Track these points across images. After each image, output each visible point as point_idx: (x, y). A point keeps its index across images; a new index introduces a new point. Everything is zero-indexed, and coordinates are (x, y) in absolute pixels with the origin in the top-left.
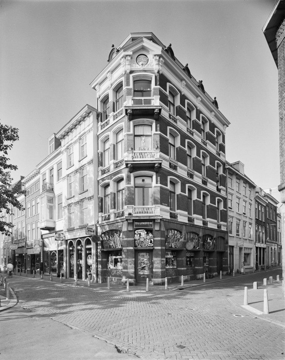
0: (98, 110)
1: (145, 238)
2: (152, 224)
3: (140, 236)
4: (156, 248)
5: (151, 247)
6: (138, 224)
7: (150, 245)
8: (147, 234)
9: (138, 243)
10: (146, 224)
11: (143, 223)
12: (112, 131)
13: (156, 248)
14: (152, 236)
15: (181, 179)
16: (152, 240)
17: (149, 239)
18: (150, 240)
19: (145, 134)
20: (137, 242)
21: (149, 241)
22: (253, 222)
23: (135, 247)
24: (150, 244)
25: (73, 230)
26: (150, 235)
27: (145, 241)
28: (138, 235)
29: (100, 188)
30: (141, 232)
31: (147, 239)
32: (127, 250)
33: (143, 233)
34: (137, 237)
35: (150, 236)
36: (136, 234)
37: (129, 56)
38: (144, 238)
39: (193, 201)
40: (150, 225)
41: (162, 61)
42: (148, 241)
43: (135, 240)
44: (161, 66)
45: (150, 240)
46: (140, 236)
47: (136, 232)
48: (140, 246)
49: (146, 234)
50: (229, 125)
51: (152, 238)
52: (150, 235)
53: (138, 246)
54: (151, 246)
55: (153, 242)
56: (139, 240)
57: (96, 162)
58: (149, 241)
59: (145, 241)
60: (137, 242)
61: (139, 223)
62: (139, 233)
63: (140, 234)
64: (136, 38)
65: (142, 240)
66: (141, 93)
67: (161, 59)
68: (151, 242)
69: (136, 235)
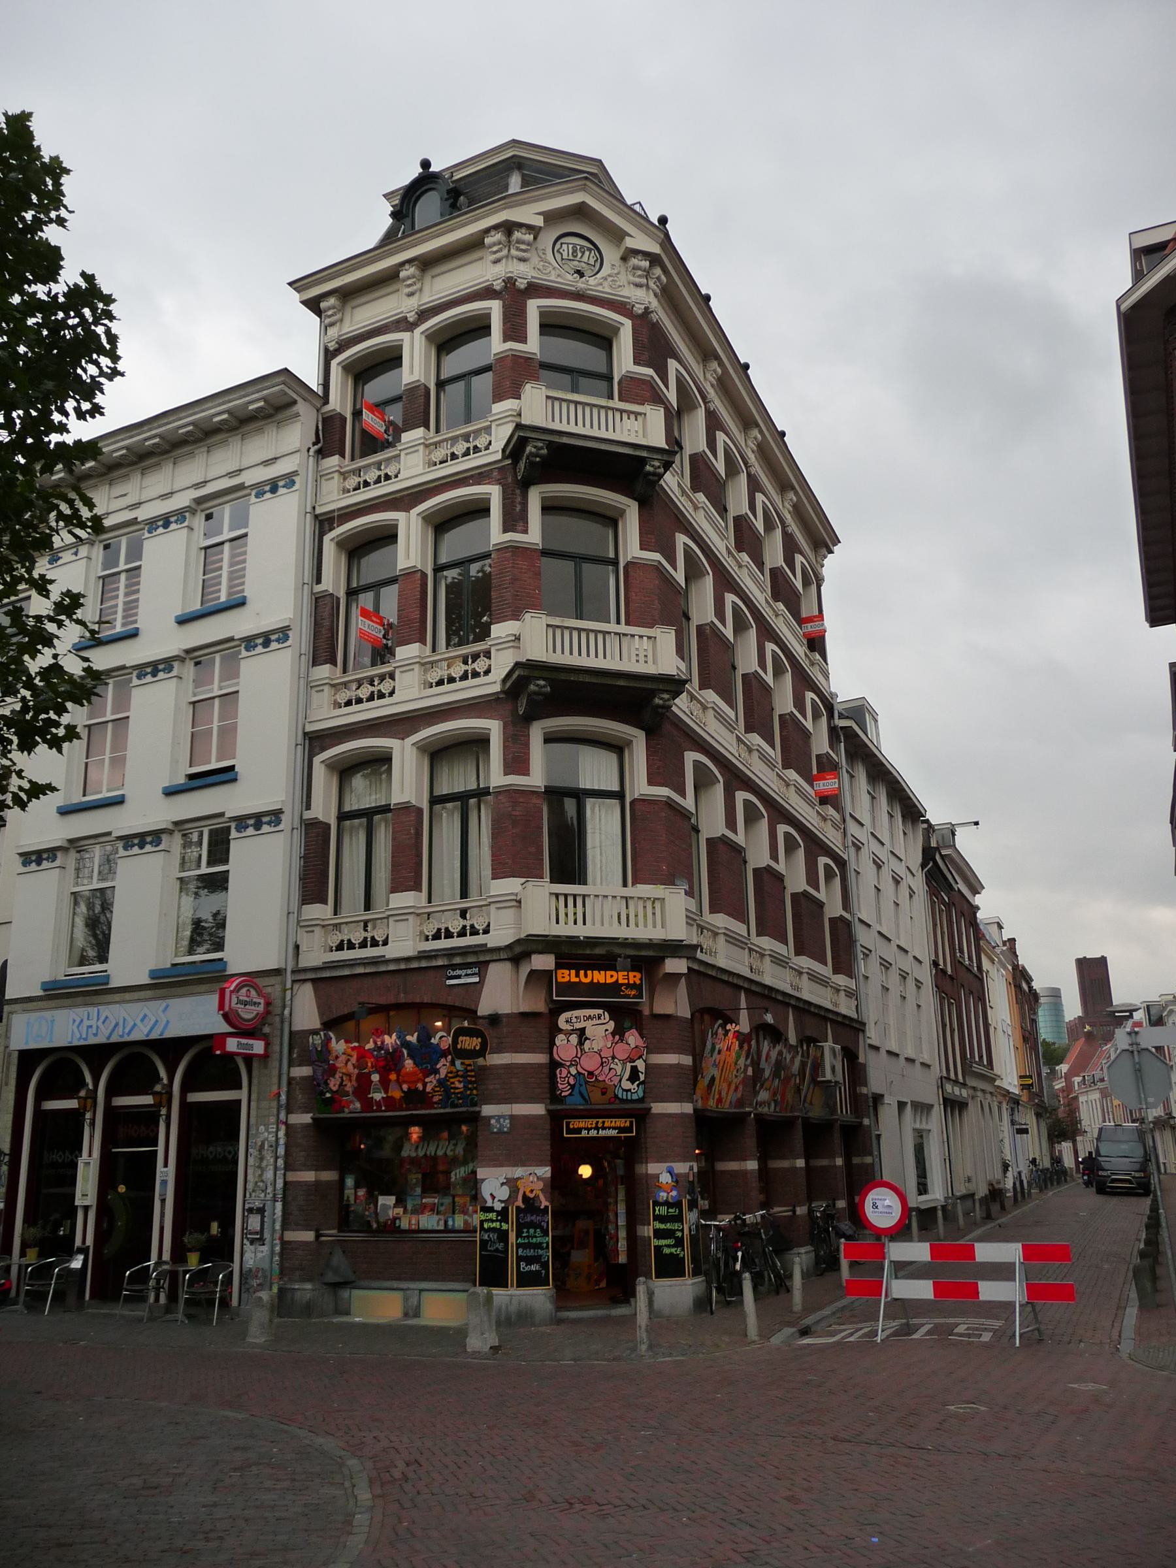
0: (326, 399)
1: (607, 1054)
2: (638, 982)
3: (581, 1043)
4: (658, 1108)
5: (632, 1101)
6: (574, 979)
7: (627, 1091)
8: (619, 1032)
9: (572, 1082)
10: (609, 981)
11: (596, 972)
12: (415, 511)
13: (658, 1108)
14: (641, 1043)
15: (730, 770)
16: (640, 1065)
17: (624, 1062)
18: (629, 1065)
19: (245, 464)
20: (565, 1072)
21: (624, 1069)
22: (925, 974)
23: (552, 1102)
24: (626, 1085)
25: (96, 993)
26: (633, 1038)
27: (606, 1069)
28: (574, 1039)
29: (319, 771)
30: (588, 1024)
31: (614, 1058)
32: (512, 1118)
33: (598, 1027)
34: (565, 1046)
35: (633, 1046)
36: (560, 1031)
37: (530, 228)
38: (599, 1053)
39: (755, 870)
40: (628, 985)
41: (658, 278)
42: (619, 1068)
43: (554, 1065)
44: (656, 295)
45: (629, 1065)
46: (581, 1043)
47: (562, 1022)
48: (577, 1099)
49: (613, 1034)
50: (836, 549)
51: (640, 1057)
52: (633, 1038)
53: (568, 1100)
54: (635, 1097)
55: (642, 1077)
56: (574, 1063)
57: (301, 638)
58: (624, 1069)
59: (606, 1069)
60: (565, 1072)
61: (577, 975)
62: (578, 1026)
63: (582, 1032)
64: (561, 171)
65: (589, 1063)
66: (567, 378)
67: (658, 271)
68: (634, 1076)
69: (560, 1039)
